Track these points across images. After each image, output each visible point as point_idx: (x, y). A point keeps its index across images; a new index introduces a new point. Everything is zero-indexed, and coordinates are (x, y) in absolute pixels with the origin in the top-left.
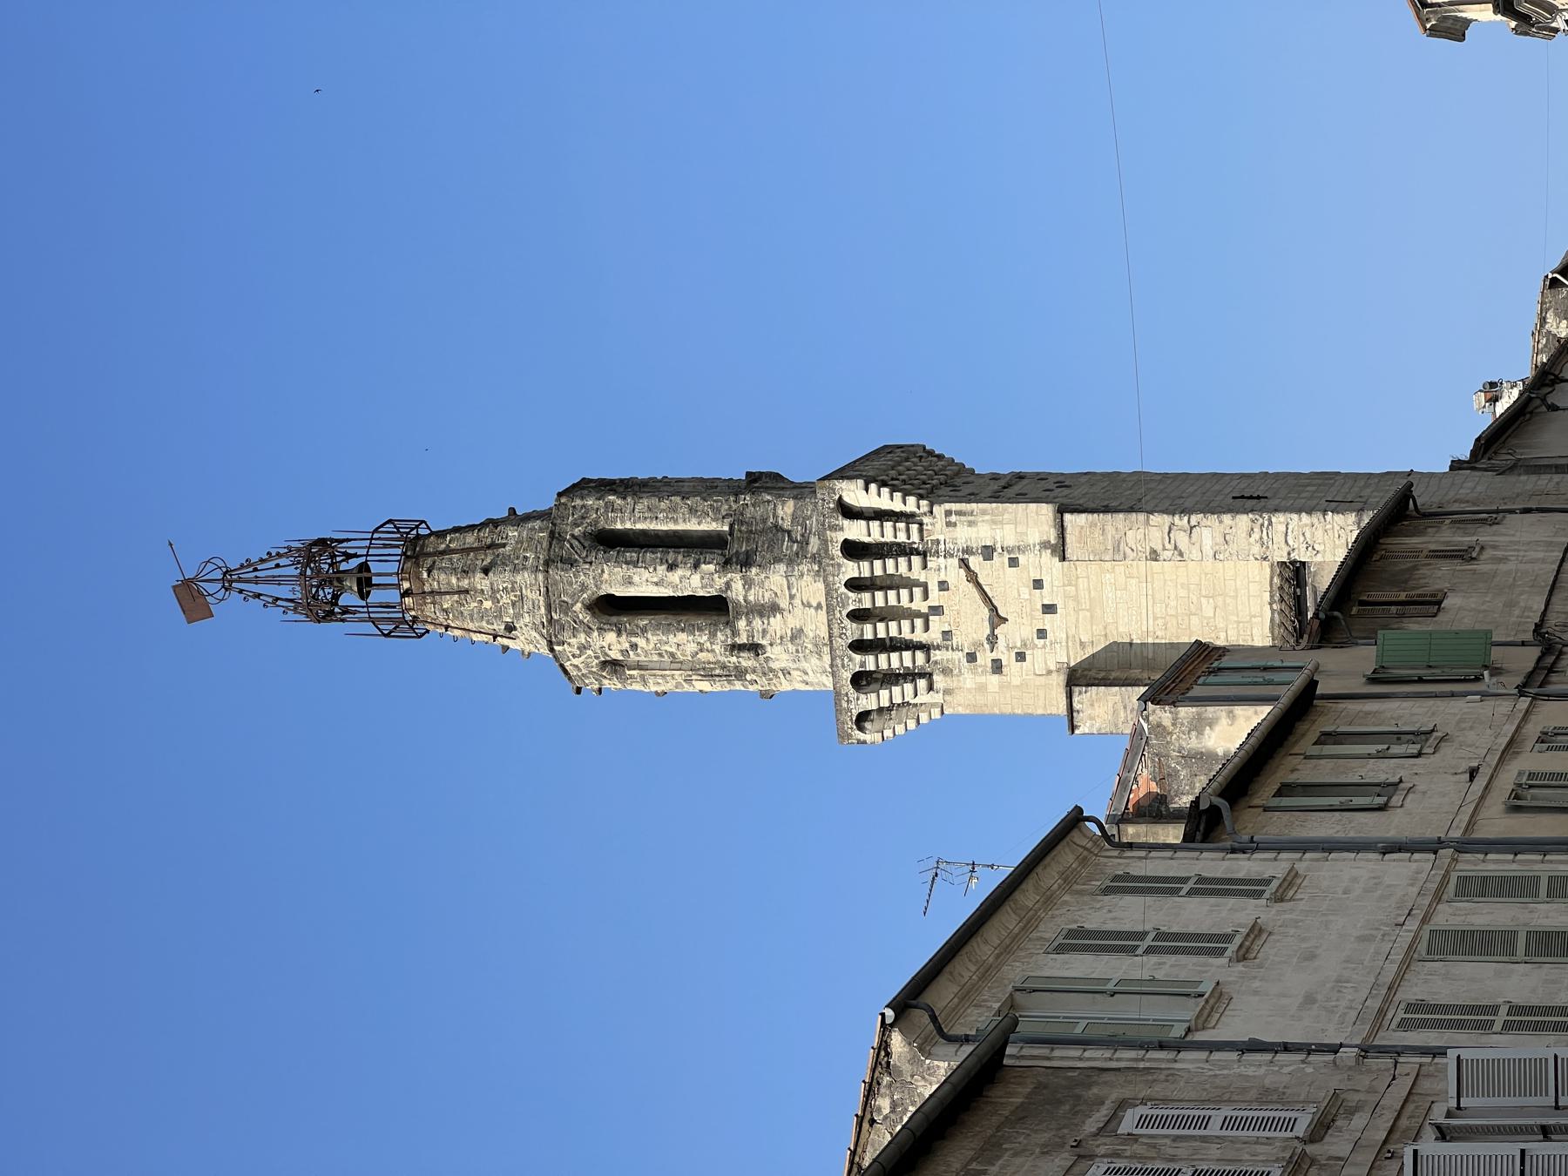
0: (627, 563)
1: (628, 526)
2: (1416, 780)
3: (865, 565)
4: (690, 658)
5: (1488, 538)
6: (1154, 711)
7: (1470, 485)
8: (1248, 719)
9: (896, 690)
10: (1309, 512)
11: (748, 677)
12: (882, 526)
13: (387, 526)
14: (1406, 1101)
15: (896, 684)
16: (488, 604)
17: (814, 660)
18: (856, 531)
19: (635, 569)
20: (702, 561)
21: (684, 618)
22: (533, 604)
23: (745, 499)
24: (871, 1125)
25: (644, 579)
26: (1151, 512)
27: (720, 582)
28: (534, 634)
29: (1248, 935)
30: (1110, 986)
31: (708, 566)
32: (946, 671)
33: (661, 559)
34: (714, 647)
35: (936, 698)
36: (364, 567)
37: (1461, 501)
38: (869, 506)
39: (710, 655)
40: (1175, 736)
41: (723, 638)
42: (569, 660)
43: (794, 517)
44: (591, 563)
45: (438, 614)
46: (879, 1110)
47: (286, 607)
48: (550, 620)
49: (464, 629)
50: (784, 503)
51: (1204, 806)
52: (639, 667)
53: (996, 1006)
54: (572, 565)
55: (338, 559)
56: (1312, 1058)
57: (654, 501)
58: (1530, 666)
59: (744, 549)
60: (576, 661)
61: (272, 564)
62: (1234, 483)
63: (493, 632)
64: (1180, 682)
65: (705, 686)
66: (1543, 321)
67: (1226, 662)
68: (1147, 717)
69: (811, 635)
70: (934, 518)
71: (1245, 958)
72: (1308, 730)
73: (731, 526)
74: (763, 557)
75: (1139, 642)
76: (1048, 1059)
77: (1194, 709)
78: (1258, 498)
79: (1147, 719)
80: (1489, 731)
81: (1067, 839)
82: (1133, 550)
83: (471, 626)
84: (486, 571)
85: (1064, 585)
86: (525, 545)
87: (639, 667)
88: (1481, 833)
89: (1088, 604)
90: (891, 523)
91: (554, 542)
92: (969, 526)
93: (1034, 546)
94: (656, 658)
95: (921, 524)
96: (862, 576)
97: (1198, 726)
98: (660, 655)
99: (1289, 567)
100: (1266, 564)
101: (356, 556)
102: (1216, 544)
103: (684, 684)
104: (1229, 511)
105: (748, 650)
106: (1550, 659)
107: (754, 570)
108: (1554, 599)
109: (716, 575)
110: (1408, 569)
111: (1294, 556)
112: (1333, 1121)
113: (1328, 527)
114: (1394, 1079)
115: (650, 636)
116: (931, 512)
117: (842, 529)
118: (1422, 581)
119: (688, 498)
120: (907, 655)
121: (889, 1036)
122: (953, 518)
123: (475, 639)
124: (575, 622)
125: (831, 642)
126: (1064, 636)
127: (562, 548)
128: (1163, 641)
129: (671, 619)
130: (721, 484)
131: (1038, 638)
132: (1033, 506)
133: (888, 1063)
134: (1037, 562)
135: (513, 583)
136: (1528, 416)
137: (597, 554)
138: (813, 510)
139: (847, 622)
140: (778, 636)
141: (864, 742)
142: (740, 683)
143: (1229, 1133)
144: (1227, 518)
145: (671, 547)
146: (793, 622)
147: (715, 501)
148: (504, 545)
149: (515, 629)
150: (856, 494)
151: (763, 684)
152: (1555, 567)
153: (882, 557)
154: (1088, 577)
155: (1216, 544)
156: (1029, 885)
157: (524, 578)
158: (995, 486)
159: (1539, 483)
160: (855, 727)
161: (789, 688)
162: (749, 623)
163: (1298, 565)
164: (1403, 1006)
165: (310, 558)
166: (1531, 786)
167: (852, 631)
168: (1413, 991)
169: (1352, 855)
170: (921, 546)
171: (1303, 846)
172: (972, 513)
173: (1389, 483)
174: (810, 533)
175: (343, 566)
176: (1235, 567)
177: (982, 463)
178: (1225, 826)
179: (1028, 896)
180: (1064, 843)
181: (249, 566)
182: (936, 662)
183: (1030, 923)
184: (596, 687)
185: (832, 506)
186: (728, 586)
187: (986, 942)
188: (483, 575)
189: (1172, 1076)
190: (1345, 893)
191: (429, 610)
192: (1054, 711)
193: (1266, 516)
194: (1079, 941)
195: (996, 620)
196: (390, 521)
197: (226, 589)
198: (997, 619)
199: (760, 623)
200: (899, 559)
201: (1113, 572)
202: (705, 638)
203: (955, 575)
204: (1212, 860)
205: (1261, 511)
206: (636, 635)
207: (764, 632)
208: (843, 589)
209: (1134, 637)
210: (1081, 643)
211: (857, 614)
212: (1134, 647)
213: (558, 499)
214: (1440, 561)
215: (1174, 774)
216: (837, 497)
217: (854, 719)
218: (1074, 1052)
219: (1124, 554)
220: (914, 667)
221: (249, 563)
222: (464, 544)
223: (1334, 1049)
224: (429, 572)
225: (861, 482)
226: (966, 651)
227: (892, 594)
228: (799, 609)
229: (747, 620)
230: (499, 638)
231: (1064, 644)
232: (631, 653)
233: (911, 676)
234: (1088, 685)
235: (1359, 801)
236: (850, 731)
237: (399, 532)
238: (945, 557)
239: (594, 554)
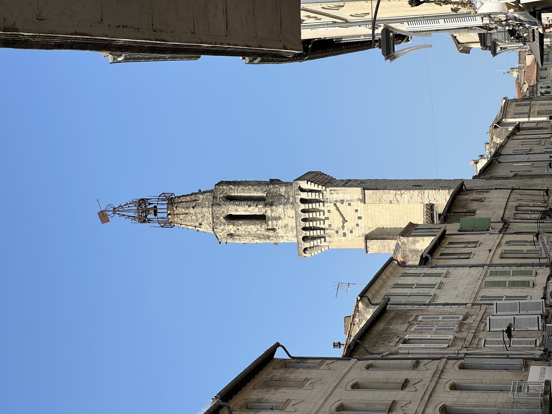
0: (236, 205)
1: (236, 194)
2: (475, 252)
3: (307, 205)
4: (254, 233)
5: (486, 196)
6: (402, 239)
7: (479, 183)
8: (427, 240)
9: (315, 241)
10: (435, 190)
11: (271, 238)
12: (312, 194)
13: (162, 195)
14: (484, 313)
15: (315, 240)
16: (194, 217)
17: (291, 233)
18: (304, 195)
19: (239, 207)
20: (258, 204)
21: (253, 221)
22: (208, 217)
23: (270, 187)
24: (354, 325)
25: (241, 210)
26: (390, 190)
28: (207, 226)
29: (440, 284)
30: (408, 294)
31: (260, 206)
32: (330, 236)
33: (246, 204)
34: (262, 229)
35: (326, 244)
36: (155, 207)
37: (477, 187)
38: (308, 188)
39: (260, 232)
40: (408, 245)
41: (264, 227)
42: (218, 234)
43: (285, 192)
44: (225, 205)
45: (178, 220)
46: (356, 321)
47: (132, 219)
48: (213, 222)
49: (186, 225)
50: (282, 187)
51: (424, 256)
52: (239, 236)
53: (381, 299)
54: (220, 206)
55: (147, 205)
56: (460, 306)
57: (244, 187)
58: (501, 227)
59: (271, 201)
60: (220, 234)
61: (127, 206)
62: (412, 182)
63: (195, 226)
64: (408, 231)
65: (258, 241)
66: (492, 138)
67: (419, 227)
68: (400, 240)
69: (290, 226)
70: (327, 192)
71: (440, 289)
72: (445, 242)
74: (276, 203)
75: (386, 227)
76: (397, 308)
77: (413, 238)
78: (420, 186)
79: (400, 241)
80: (493, 242)
81: (390, 264)
82: (385, 201)
83: (188, 224)
84: (193, 208)
85: (364, 211)
86: (205, 200)
87: (239, 236)
88: (494, 262)
89: (371, 216)
90: (314, 193)
91: (214, 199)
92: (337, 194)
93: (356, 200)
94: (244, 233)
95: (323, 194)
96: (306, 208)
97: (414, 242)
98: (246, 232)
99: (429, 205)
100: (423, 204)
101: (152, 204)
102: (409, 199)
103: (252, 240)
104: (412, 189)
105: (272, 230)
106: (506, 226)
107: (274, 207)
108: (506, 211)
109: (263, 209)
110: (465, 204)
111: (431, 202)
112: (468, 317)
113: (441, 194)
114: (481, 309)
115: (243, 226)
116: (326, 190)
117: (300, 195)
118: (469, 207)
119: (254, 186)
120: (318, 231)
121: (359, 303)
122: (332, 192)
123: (189, 228)
124: (221, 222)
125: (296, 228)
126: (364, 226)
127: (217, 201)
128: (393, 227)
129: (249, 221)
130: (263, 182)
131: (356, 226)
132: (355, 188)
133: (358, 310)
134: (356, 204)
136: (492, 164)
137: (227, 202)
138: (291, 190)
139: (301, 222)
140: (281, 226)
141: (306, 257)
142: (268, 240)
143: (444, 320)
144: (412, 191)
145: (249, 200)
147: (261, 187)
148: (199, 200)
149: (202, 224)
150: (304, 184)
151: (275, 240)
152: (506, 203)
153: (311, 203)
154: (371, 209)
155: (409, 199)
156: (383, 274)
157: (205, 210)
158: (343, 183)
159: (498, 182)
160: (303, 252)
161: (283, 242)
162: (272, 222)
163: (432, 205)
164: (480, 297)
165: (140, 205)
166: (505, 253)
167: (303, 224)
168: (482, 293)
169: (462, 268)
170: (323, 200)
171: (450, 266)
173: (456, 182)
174: (290, 196)
175: (148, 207)
176: (413, 206)
177: (338, 177)
178: (429, 262)
179: (383, 276)
180: (389, 265)
181: (121, 207)
182: (327, 234)
183: (385, 282)
184: (225, 242)
185: (297, 188)
186: (266, 212)
187: (376, 285)
188: (193, 209)
189: (427, 311)
190: (462, 276)
191: (176, 219)
193: (423, 191)
194: (397, 286)
195: (344, 221)
196: (163, 193)
197: (114, 214)
198: (345, 221)
199: (275, 222)
200: (317, 204)
201: (378, 207)
202: (259, 227)
203: (333, 208)
204: (427, 270)
205: (421, 189)
206: (238, 226)
207: (276, 225)
208: (300, 212)
209: (384, 226)
210: (369, 228)
211: (304, 220)
212: (384, 229)
213: (215, 187)
214: (474, 202)
215: (407, 256)
216: (299, 186)
217: (303, 250)
218: (403, 306)
219: (382, 202)
220: (320, 235)
221: (120, 206)
222: (186, 200)
223: (466, 304)
224: (176, 208)
225: (306, 181)
226: (335, 230)
227: (314, 214)
229: (272, 221)
230: (196, 228)
231: (364, 228)
232: (237, 231)
233: (319, 237)
234: (371, 240)
235: (462, 257)
236: (302, 253)
237: (165, 196)
238: (330, 203)
239: (226, 202)
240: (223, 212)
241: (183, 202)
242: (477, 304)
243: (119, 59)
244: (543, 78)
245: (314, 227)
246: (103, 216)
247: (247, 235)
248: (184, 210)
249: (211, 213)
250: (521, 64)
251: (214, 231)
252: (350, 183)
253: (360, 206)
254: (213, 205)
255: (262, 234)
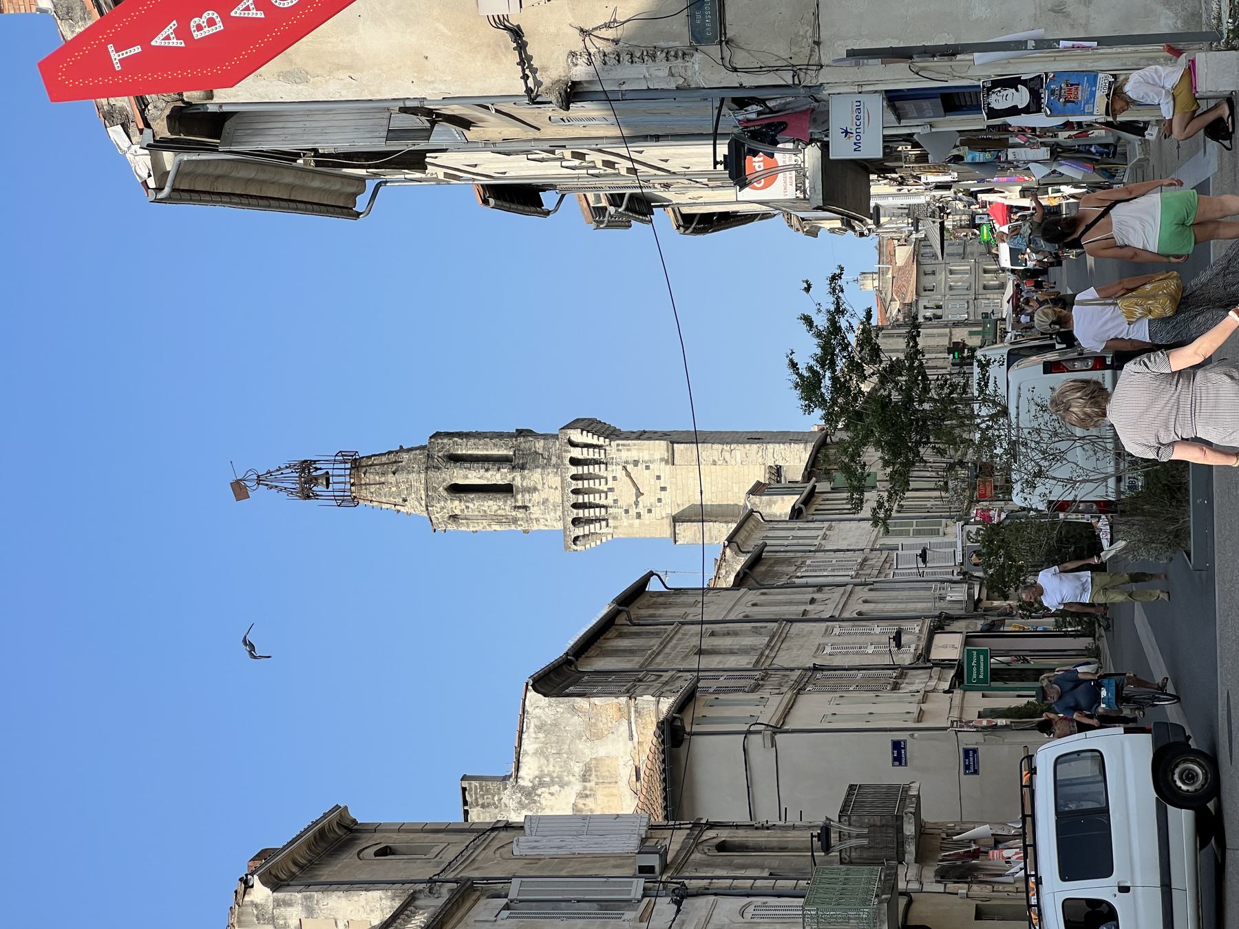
1: (464, 452)
3: (580, 468)
8: (789, 500)
9: (592, 526)
10: (784, 443)
16: (394, 489)
17: (552, 514)
18: (576, 453)
26: (713, 443)
27: (510, 477)
28: (416, 503)
32: (615, 518)
35: (611, 530)
43: (544, 448)
48: (427, 496)
57: (477, 440)
60: (437, 515)
61: (280, 472)
69: (552, 501)
73: (515, 451)
79: (749, 501)
83: (384, 500)
84: (394, 473)
94: (477, 513)
97: (770, 504)
98: (479, 512)
101: (321, 469)
107: (526, 471)
111: (777, 463)
117: (570, 452)
122: (620, 447)
127: (433, 462)
129: (484, 495)
132: (657, 441)
135: (407, 479)
139: (571, 494)
146: (544, 496)
150: (576, 436)
151: (525, 526)
156: (746, 524)
157: (413, 476)
162: (523, 496)
167: (573, 499)
172: (629, 445)
175: (314, 474)
186: (514, 479)
192: (664, 536)
198: (639, 494)
203: (620, 473)
205: (763, 443)
206: (467, 501)
207: (530, 500)
208: (570, 480)
218: (783, 554)
223: (863, 550)
225: (579, 430)
227: (591, 482)
228: (546, 490)
233: (598, 520)
240: (444, 480)
241: (376, 465)
242: (876, 550)
243: (601, 226)
244: (929, 290)
245: (590, 503)
246: (239, 489)
247: (480, 518)
248: (377, 478)
249: (423, 482)
250: (883, 264)
251: (427, 509)
252: (646, 436)
253: (665, 470)
254: (427, 468)
255: (506, 515)
